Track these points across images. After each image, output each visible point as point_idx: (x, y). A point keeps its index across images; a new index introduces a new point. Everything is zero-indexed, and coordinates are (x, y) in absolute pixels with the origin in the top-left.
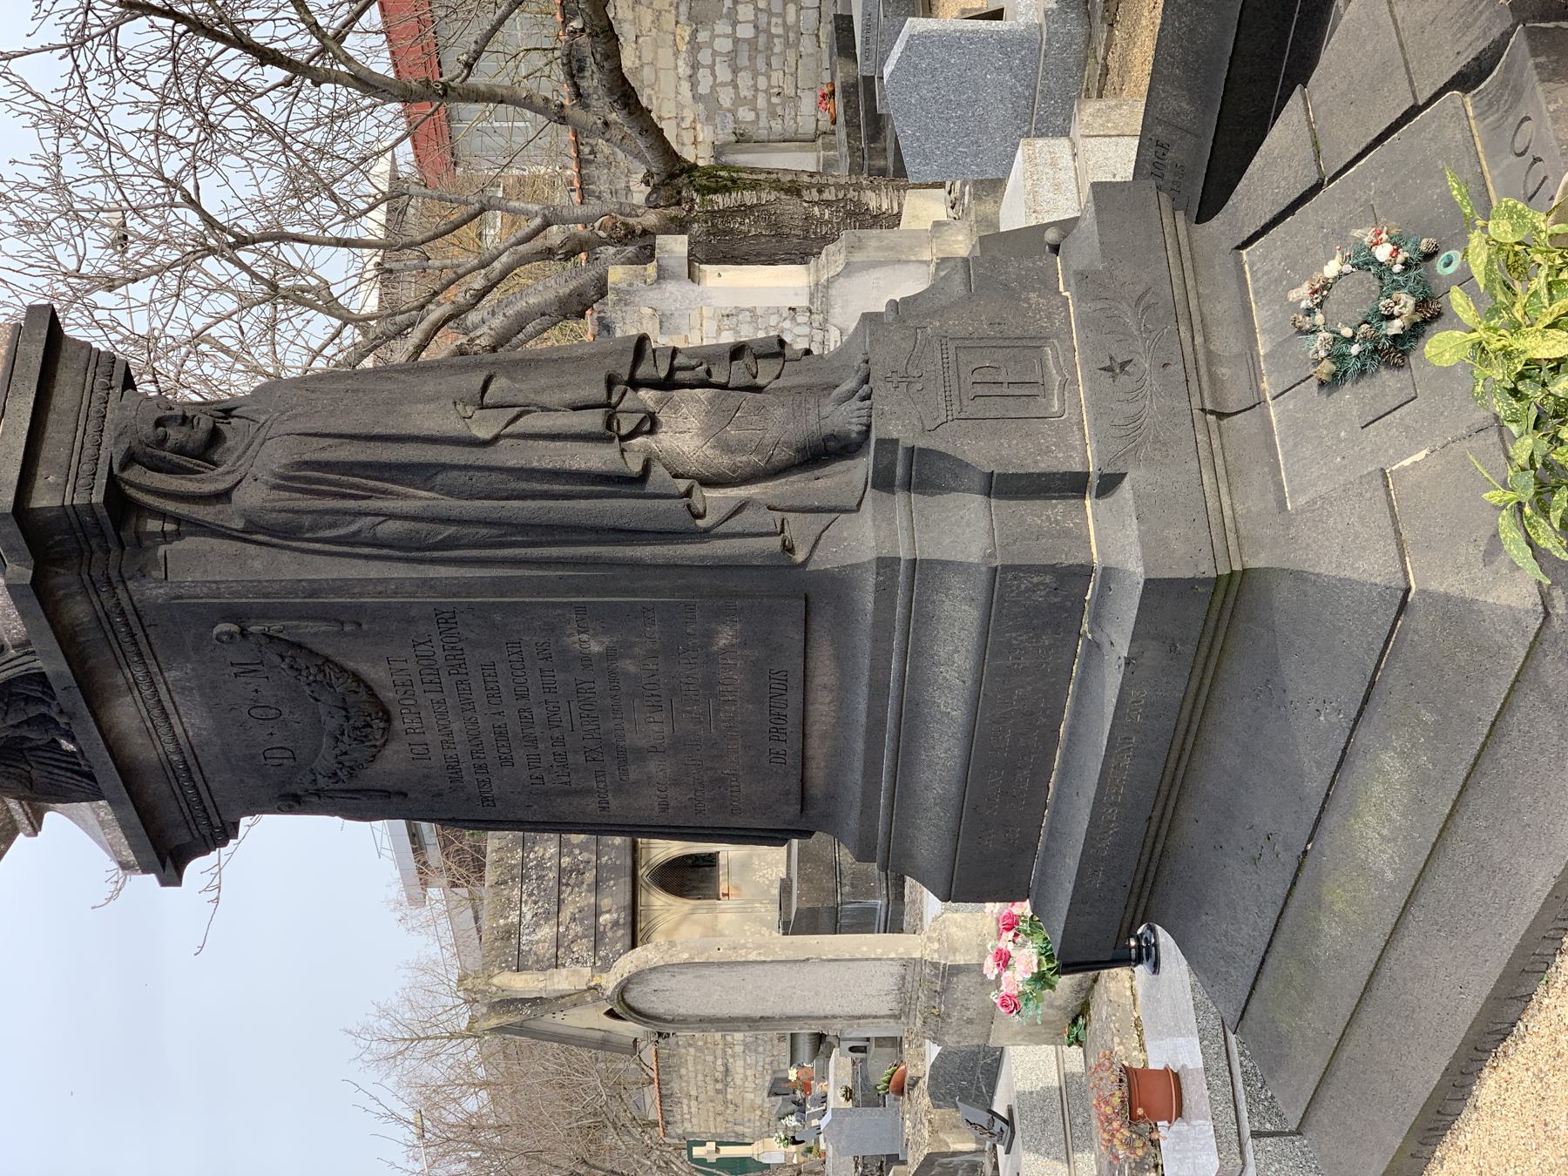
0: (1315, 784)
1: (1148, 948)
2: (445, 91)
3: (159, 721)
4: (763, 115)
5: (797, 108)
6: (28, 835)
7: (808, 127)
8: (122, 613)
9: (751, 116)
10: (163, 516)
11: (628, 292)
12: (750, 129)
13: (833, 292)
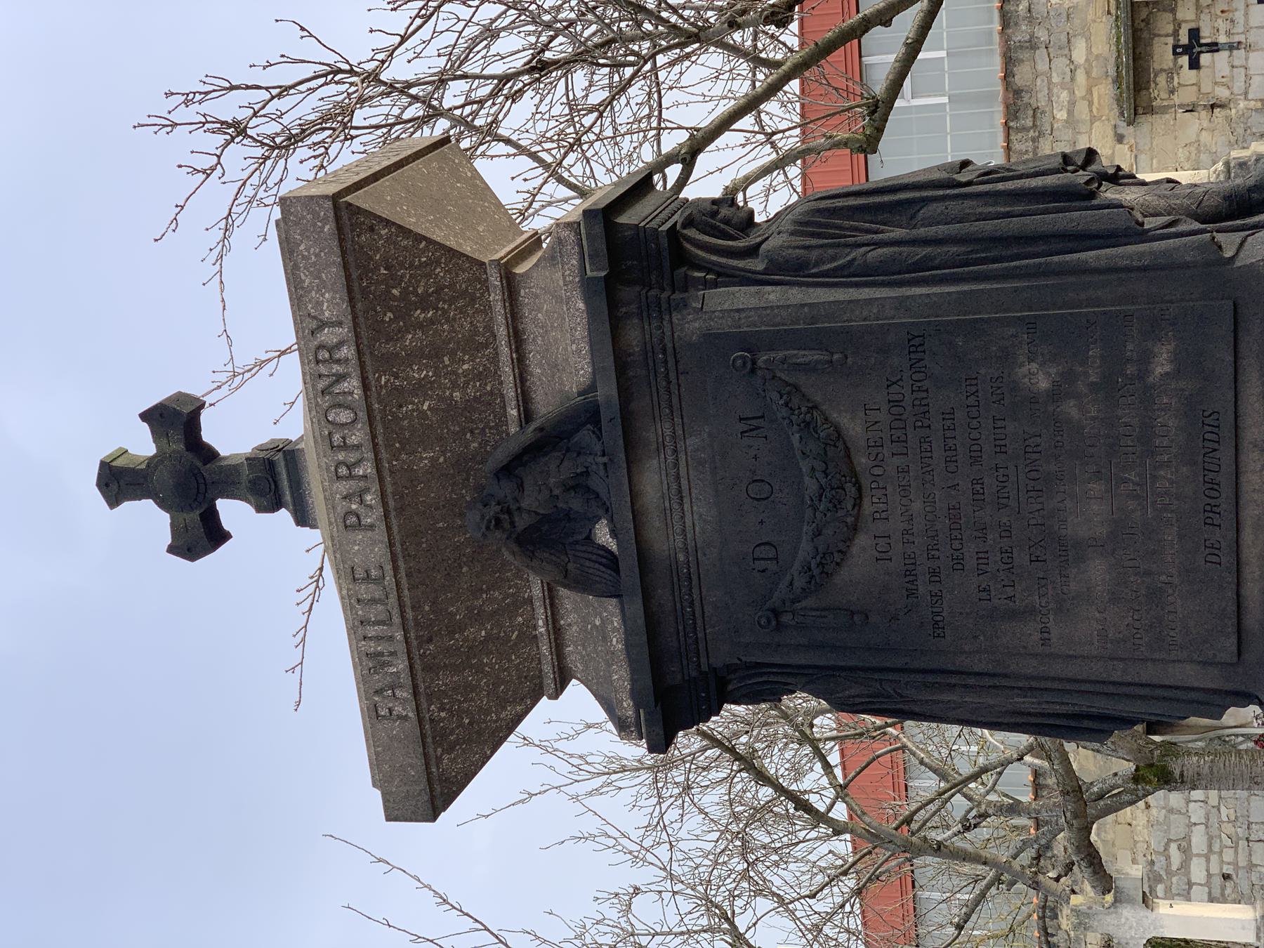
2: (939, 847)
3: (675, 499)
6: (550, 698)
8: (664, 351)
11: (1088, 915)
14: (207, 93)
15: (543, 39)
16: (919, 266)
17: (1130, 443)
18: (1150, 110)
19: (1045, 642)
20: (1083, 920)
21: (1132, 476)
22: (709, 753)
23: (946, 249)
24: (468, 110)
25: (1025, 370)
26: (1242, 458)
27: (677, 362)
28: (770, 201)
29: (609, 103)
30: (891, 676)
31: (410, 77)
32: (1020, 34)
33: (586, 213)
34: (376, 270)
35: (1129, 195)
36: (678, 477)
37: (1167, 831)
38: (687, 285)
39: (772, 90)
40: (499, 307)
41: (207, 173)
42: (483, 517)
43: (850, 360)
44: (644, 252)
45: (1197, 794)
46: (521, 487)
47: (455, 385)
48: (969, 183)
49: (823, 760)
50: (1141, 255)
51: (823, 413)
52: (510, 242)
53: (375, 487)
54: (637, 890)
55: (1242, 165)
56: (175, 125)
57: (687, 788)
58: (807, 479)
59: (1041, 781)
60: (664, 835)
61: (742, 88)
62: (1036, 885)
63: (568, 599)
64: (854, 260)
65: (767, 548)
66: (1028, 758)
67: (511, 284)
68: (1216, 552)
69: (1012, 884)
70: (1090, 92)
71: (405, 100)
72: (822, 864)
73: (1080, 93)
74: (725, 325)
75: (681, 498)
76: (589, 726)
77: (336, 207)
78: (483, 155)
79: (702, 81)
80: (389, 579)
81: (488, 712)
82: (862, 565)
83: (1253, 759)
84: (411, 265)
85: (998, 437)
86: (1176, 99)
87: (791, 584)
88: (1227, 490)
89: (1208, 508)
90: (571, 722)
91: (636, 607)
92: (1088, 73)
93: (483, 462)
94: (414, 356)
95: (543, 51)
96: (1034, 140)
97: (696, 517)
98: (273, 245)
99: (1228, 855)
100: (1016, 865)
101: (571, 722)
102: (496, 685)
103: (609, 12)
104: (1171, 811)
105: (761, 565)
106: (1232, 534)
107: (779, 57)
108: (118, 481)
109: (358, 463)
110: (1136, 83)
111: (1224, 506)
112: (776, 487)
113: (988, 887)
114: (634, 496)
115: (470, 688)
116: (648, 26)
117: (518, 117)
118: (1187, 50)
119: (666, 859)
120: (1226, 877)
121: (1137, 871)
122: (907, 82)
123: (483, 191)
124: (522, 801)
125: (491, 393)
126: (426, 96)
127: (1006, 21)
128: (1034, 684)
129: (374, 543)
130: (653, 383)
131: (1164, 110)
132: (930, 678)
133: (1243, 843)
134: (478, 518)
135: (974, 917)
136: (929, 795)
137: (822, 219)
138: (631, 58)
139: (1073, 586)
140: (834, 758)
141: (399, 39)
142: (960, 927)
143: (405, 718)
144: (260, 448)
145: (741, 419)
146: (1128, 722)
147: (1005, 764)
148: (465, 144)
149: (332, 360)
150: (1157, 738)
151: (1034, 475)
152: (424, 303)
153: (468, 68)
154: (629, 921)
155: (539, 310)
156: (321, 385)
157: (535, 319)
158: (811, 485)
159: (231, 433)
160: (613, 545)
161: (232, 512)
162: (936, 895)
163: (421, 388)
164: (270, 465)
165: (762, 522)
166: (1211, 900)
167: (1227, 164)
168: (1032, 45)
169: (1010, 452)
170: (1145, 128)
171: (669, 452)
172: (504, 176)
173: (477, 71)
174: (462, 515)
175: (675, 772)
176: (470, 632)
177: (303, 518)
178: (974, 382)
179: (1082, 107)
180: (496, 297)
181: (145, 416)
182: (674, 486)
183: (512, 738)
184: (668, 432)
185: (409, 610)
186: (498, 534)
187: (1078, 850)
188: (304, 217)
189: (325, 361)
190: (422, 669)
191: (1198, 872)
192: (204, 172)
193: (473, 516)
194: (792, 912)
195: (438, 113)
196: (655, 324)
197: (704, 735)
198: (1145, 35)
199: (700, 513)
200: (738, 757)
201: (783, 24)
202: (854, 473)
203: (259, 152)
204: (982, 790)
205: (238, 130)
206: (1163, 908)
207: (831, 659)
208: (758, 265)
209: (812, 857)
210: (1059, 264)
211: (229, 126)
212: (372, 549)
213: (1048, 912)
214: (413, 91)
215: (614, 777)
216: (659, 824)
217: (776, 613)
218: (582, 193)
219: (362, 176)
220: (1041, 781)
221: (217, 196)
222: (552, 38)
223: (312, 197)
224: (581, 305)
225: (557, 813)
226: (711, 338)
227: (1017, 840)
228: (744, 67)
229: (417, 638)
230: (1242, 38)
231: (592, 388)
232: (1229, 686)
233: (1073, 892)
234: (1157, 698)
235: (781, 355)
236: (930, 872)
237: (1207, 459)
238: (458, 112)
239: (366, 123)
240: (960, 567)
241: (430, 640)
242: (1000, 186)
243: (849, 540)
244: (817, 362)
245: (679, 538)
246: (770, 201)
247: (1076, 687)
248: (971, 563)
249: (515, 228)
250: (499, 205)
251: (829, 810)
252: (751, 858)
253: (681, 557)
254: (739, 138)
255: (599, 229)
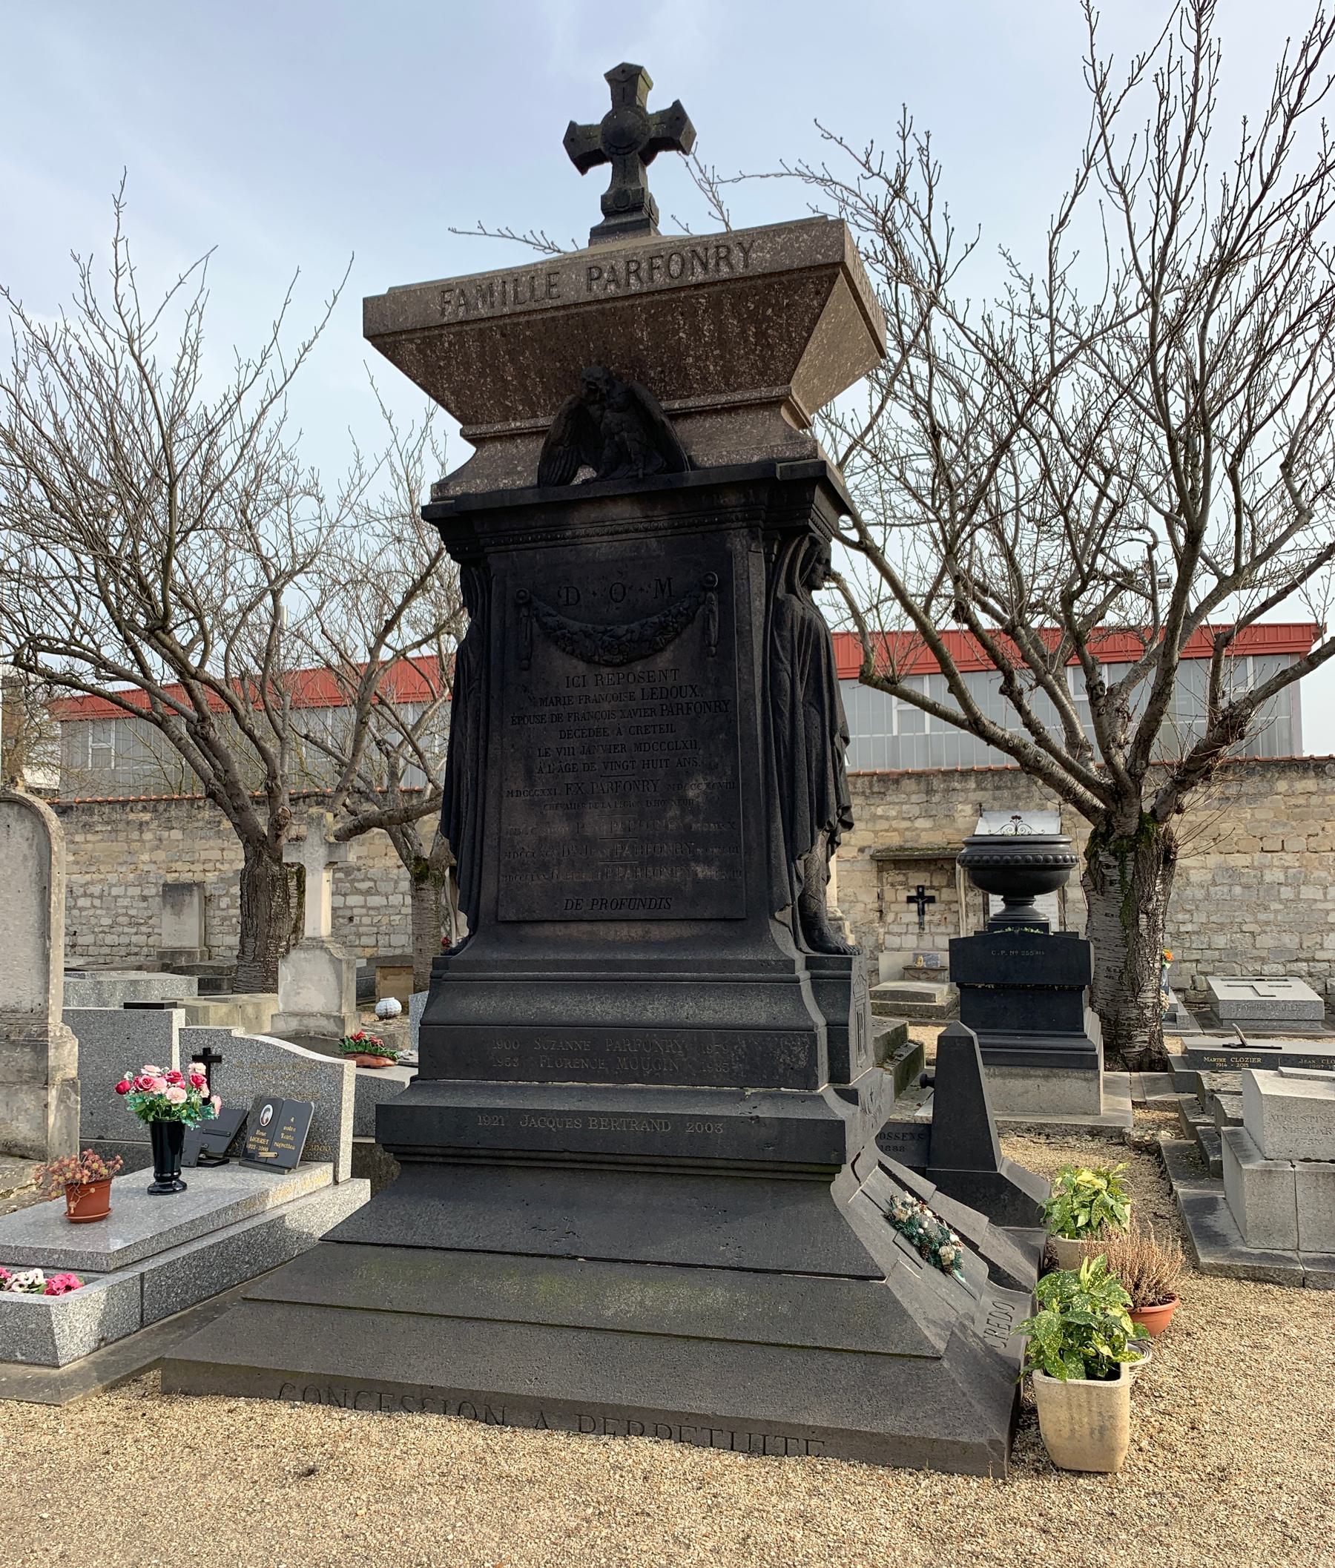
0: (652, 1253)
1: (170, 1186)
3: (611, 529)
4: (224, 913)
5: (228, 934)
7: (214, 941)
9: (223, 905)
10: (780, 556)
12: (214, 905)
13: (318, 952)
14: (927, 166)
15: (956, 437)
16: (777, 709)
18: (880, 870)
20: (317, 822)
21: (627, 852)
22: (426, 557)
24: (907, 377)
25: (701, 780)
27: (712, 532)
28: (825, 599)
29: (908, 488)
30: (483, 687)
31: (933, 332)
32: (937, 784)
33: (823, 464)
34: (787, 295)
35: (819, 850)
36: (627, 531)
37: (382, 880)
38: (768, 541)
39: (909, 609)
40: (756, 394)
41: (866, 165)
42: (598, 379)
44: (795, 505)
45: (409, 900)
46: (619, 410)
47: (697, 358)
48: (833, 743)
49: (424, 641)
50: (778, 858)
51: (673, 639)
52: (805, 404)
53: (621, 293)
54: (321, 500)
55: (839, 929)
56: (904, 138)
57: (399, 540)
58: (626, 627)
59: (415, 795)
60: (363, 522)
61: (911, 587)
62: (339, 790)
63: (537, 446)
66: (430, 786)
67: (772, 404)
69: (340, 774)
70: (895, 830)
71: (916, 327)
72: (348, 640)
73: (894, 824)
74: (737, 568)
76: (443, 465)
77: (835, 265)
78: (873, 388)
79: (918, 557)
80: (550, 303)
81: (449, 381)
82: (563, 666)
83: (434, 936)
84: (789, 325)
86: (887, 888)
90: (445, 447)
91: (530, 498)
92: (907, 829)
93: (640, 380)
94: (721, 327)
95: (947, 435)
96: (863, 793)
98: (809, 214)
99: (366, 920)
100: (353, 777)
101: (445, 447)
102: (469, 388)
103: (973, 488)
104: (396, 882)
105: (563, 592)
106: (586, 917)
107: (932, 614)
108: (626, 81)
109: (639, 278)
110: (899, 861)
112: (619, 605)
113: (337, 757)
114: (614, 499)
115: (467, 366)
116: (960, 516)
117: (899, 415)
118: (921, 895)
119: (346, 522)
120: (351, 919)
121: (352, 858)
122: (910, 706)
123: (843, 384)
124: (384, 412)
125: (691, 388)
126: (918, 345)
127: (948, 774)
128: (480, 786)
129: (577, 292)
131: (880, 879)
133: (375, 930)
134: (598, 375)
135: (315, 747)
136: (401, 717)
137: (813, 638)
138: (937, 504)
139: (550, 813)
140: (426, 651)
141: (961, 321)
142: (306, 737)
143: (443, 314)
144: (651, 200)
146: (455, 848)
147: (426, 770)
148: (881, 374)
149: (718, 259)
150: (447, 873)
151: (628, 786)
152: (761, 334)
153: (937, 377)
154: (297, 493)
155: (753, 426)
156: (700, 250)
157: (746, 423)
159: (664, 176)
160: (577, 481)
161: (602, 175)
162: (329, 722)
163: (696, 332)
164: (638, 207)
165: (594, 594)
166: (334, 909)
167: (841, 919)
168: (930, 792)
170: (868, 867)
172: (855, 401)
173: (935, 385)
174: (599, 363)
175: (410, 531)
176: (510, 368)
177: (597, 233)
179: (885, 825)
180: (764, 392)
181: (677, 105)
183: (433, 402)
184: (661, 524)
185: (526, 318)
186: (584, 391)
187: (366, 819)
188: (828, 238)
189: (718, 253)
190: (482, 329)
191: (354, 900)
192: (867, 162)
193: (598, 372)
194: (311, 617)
195: (905, 354)
197: (439, 554)
198: (932, 867)
199: (602, 548)
200: (423, 579)
201: (956, 615)
202: (630, 661)
203: (881, 208)
204: (407, 756)
205: (899, 192)
206: (326, 876)
207: (495, 644)
208: (781, 593)
209: (352, 633)
210: (774, 804)
211: (902, 184)
212: (572, 290)
213: (321, 799)
214: (922, 334)
215: (405, 484)
216: (370, 517)
217: (528, 604)
218: (840, 465)
219: (859, 287)
220: (415, 795)
221: (847, 172)
222: (956, 443)
223: (843, 245)
224: (755, 459)
225: (375, 441)
226: (729, 557)
227: (373, 778)
228: (927, 588)
229: (505, 325)
230: (927, 930)
231: (694, 467)
232: (482, 915)
233: (335, 816)
234: (472, 868)
235: (716, 609)
236: (346, 717)
238: (905, 368)
239: (900, 296)
241: (503, 335)
242: (830, 764)
243: (582, 657)
246: (825, 599)
247: (479, 814)
249: (815, 409)
250: (833, 396)
251: (388, 646)
252: (349, 587)
253: (569, 533)
254: (875, 585)
255: (811, 472)
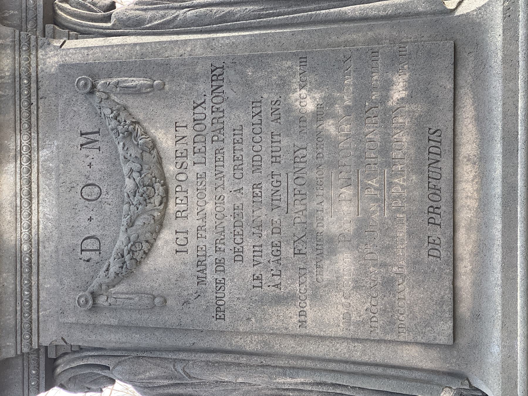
8: (29, 78)
16: (223, 19)
17: (373, 155)
19: (302, 324)
21: (373, 182)
23: (244, 8)
25: (296, 95)
26: (458, 169)
27: (38, 89)
36: (30, 182)
43: (167, 87)
58: (127, 179)
64: (177, 16)
65: (93, 240)
68: (437, 247)
74: (77, 58)
75: (31, 199)
85: (274, 149)
87: (107, 270)
88: (446, 196)
89: (431, 210)
97: (41, 215)
105: (86, 255)
111: (443, 208)
112: (104, 190)
130: (18, 102)
132: (212, 357)
145: (82, 134)
158: (129, 184)
169: (282, 162)
171: (25, 159)
178: (259, 104)
182: (25, 188)
184: (25, 143)
196: (24, 56)
210: (326, 15)
237: (431, 169)
240: (240, 258)
243: (156, 233)
244: (142, 86)
245: (25, 231)
248: (248, 254)
253: (25, 247)
